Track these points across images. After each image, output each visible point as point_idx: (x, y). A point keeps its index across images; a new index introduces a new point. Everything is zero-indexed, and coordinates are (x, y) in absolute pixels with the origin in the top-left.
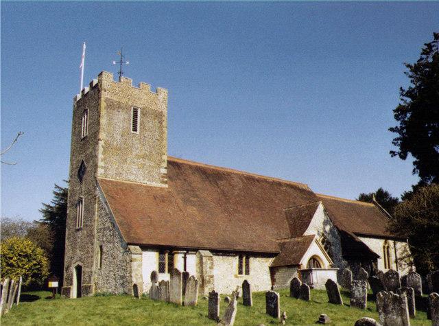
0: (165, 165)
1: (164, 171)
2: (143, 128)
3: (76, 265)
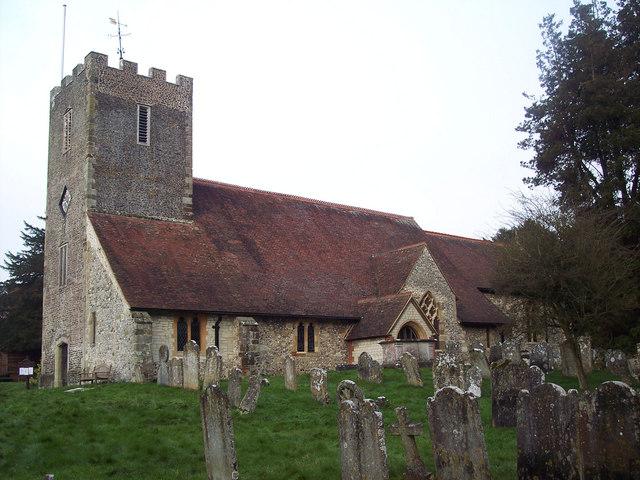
0: (189, 192)
1: (188, 201)
2: (156, 138)
3: (58, 342)
